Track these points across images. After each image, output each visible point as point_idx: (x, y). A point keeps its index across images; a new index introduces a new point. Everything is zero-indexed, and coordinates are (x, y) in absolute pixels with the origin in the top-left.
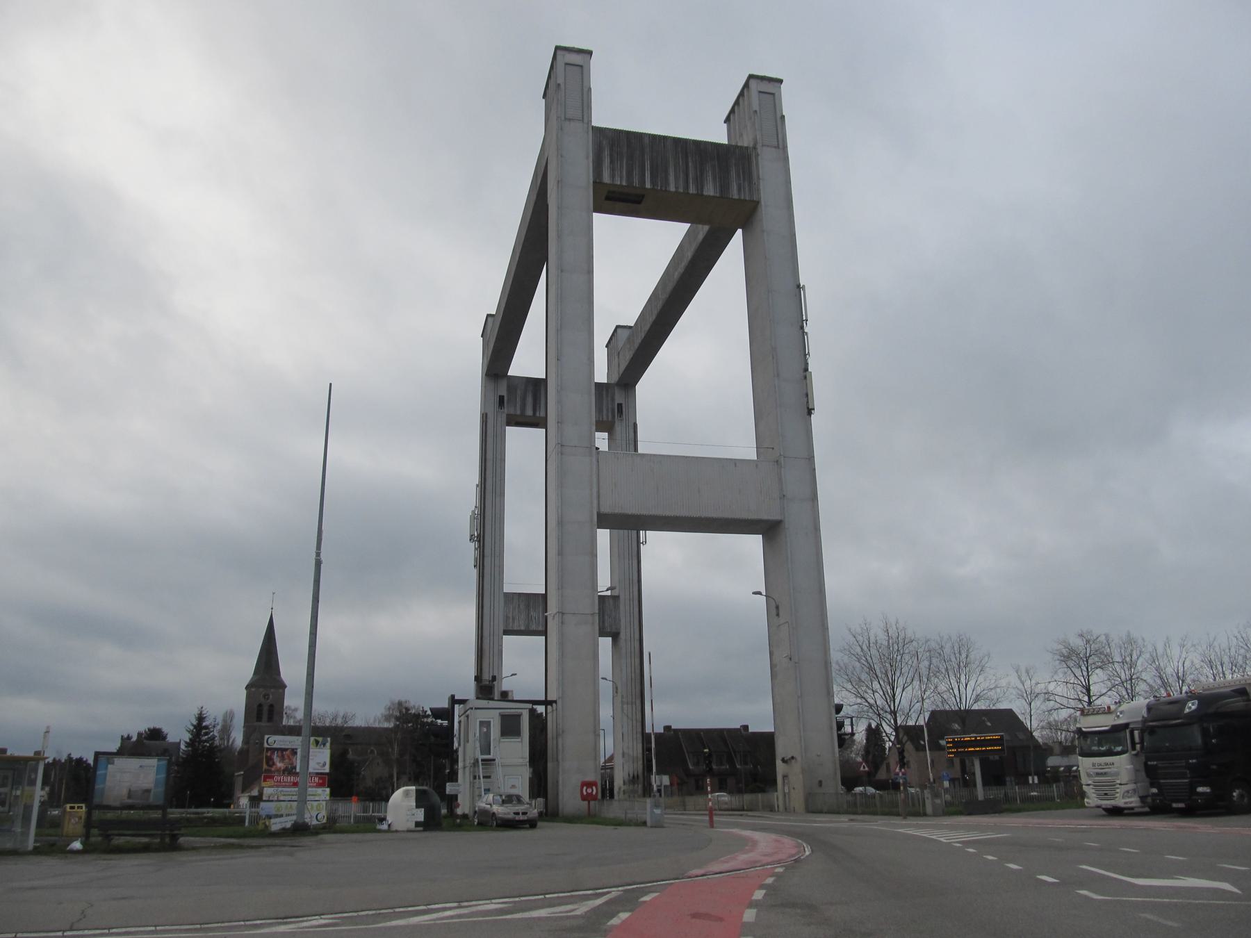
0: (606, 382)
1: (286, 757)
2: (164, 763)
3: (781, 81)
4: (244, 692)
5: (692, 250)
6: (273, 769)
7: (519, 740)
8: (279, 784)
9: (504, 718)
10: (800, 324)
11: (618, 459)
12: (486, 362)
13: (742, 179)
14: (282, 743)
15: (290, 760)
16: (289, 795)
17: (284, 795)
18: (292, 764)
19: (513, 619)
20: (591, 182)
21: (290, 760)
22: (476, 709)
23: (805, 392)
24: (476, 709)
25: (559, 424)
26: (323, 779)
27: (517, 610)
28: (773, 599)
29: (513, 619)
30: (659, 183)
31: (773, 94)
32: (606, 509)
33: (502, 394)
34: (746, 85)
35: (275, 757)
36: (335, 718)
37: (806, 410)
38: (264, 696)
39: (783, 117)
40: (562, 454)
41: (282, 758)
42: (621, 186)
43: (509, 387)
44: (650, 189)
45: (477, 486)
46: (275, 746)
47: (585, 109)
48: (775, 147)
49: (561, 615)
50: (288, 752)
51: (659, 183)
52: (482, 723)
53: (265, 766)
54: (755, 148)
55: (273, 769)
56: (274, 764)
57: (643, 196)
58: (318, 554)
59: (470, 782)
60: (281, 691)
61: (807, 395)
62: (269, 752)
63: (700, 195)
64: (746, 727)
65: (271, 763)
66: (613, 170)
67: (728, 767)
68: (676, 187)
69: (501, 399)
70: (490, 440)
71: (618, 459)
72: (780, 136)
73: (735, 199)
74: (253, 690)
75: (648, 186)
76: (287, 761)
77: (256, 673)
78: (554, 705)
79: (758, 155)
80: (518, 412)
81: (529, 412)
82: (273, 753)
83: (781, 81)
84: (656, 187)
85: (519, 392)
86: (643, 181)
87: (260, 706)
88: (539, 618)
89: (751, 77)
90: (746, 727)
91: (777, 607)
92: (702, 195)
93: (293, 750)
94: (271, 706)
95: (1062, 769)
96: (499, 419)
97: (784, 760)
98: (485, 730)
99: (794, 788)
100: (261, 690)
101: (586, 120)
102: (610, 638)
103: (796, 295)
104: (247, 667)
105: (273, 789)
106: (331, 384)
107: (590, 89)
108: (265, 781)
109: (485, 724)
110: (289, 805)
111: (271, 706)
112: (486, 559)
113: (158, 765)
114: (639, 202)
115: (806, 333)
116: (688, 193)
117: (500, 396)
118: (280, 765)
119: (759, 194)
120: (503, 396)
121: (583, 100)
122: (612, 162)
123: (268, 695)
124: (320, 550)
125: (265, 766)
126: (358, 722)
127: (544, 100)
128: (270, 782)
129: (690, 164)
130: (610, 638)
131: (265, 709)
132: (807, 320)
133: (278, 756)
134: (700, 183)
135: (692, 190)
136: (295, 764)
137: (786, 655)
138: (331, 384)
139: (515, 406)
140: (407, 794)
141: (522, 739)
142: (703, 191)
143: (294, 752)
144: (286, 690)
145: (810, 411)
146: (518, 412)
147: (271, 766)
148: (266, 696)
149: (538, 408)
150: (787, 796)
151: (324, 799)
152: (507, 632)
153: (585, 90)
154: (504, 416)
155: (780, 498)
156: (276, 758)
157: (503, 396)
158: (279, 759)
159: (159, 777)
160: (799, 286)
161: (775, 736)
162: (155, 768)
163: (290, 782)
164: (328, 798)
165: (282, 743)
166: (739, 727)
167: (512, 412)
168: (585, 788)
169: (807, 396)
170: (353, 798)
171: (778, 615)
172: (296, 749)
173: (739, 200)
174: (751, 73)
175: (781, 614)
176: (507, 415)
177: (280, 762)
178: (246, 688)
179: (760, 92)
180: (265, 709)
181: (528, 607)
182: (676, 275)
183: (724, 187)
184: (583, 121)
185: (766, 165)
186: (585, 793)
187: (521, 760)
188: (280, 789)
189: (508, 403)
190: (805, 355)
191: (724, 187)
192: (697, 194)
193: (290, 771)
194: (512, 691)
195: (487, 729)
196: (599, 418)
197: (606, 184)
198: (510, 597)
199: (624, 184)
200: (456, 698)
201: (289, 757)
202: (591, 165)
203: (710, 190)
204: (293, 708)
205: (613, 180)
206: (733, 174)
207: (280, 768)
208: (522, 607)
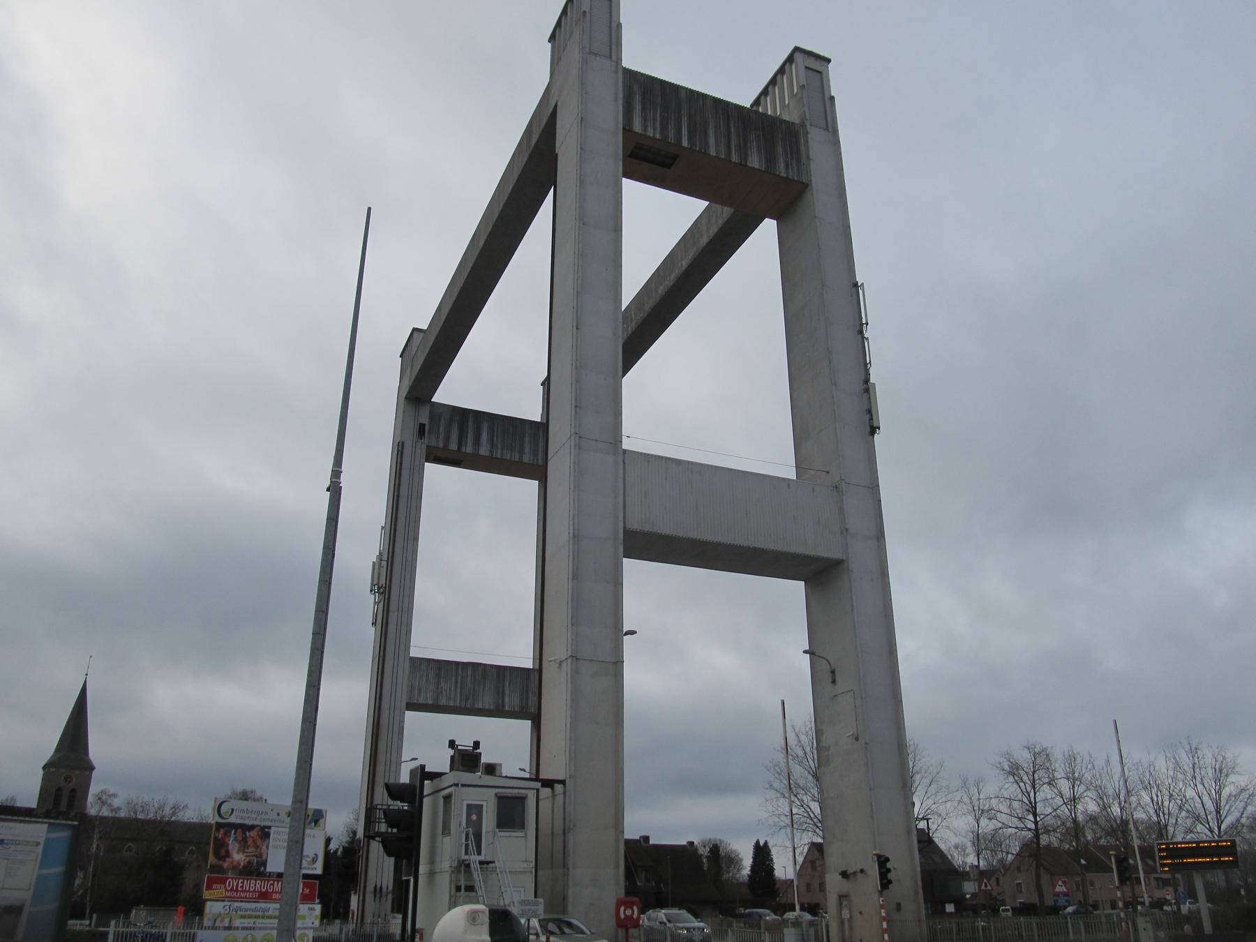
0: (539, 421)
1: (250, 841)
2: (64, 834)
3: (829, 61)
4: (41, 772)
5: (690, 257)
6: (225, 865)
7: (522, 834)
8: (235, 894)
9: (501, 799)
10: (858, 328)
11: (648, 461)
12: (407, 383)
13: (789, 156)
14: (244, 815)
15: (257, 847)
16: (250, 917)
17: (243, 917)
18: (261, 856)
19: (420, 690)
20: (621, 126)
21: (257, 847)
22: (462, 785)
23: (866, 407)
24: (462, 785)
25: (578, 409)
26: (311, 887)
27: (424, 679)
28: (827, 660)
29: (420, 690)
30: (698, 144)
31: (820, 73)
32: (634, 525)
33: (424, 422)
34: (790, 60)
35: (231, 841)
36: (161, 807)
37: (868, 429)
38: (66, 778)
39: (832, 98)
40: (579, 448)
41: (244, 845)
42: (654, 139)
43: (431, 413)
44: (687, 148)
45: (382, 528)
46: (233, 819)
47: (614, 47)
48: (824, 129)
49: (575, 659)
50: (254, 833)
51: (698, 144)
52: (470, 807)
53: (212, 859)
54: (803, 125)
55: (225, 865)
56: (228, 855)
57: (675, 157)
58: (336, 473)
59: (451, 896)
60: (87, 773)
61: (869, 412)
62: (222, 831)
63: (743, 165)
64: (646, 839)
65: (223, 853)
66: (645, 119)
67: (654, 884)
68: (717, 153)
69: (422, 427)
70: (405, 473)
71: (648, 461)
72: (829, 118)
73: (783, 177)
74: (52, 770)
75: (685, 143)
76: (251, 850)
77: (58, 749)
78: (558, 787)
79: (807, 133)
80: (441, 445)
81: (453, 446)
82: (227, 834)
83: (829, 61)
84: (694, 148)
85: (443, 422)
86: (679, 139)
87: (59, 789)
88: (450, 690)
89: (797, 49)
90: (646, 839)
91: (833, 672)
92: (746, 166)
93: (263, 828)
94: (73, 791)
95: (968, 896)
96: (418, 451)
97: (844, 875)
98: (474, 817)
99: (861, 913)
100: (63, 770)
101: (614, 58)
102: (529, 722)
103: (851, 295)
104: (49, 739)
105: (222, 904)
106: (369, 209)
107: (619, 25)
108: (209, 888)
109: (475, 810)
110: (249, 938)
111: (73, 791)
112: (390, 614)
113: (47, 841)
114: (669, 166)
115: (867, 339)
116: (730, 161)
117: (420, 424)
118: (238, 857)
119: (808, 173)
120: (424, 425)
121: (611, 35)
122: (643, 109)
123: (70, 777)
124: (340, 466)
125: (212, 859)
126: (190, 815)
127: (550, 44)
128: (219, 891)
129: (732, 130)
130: (529, 722)
131: (65, 794)
132: (867, 324)
133: (236, 839)
134: (743, 150)
135: (735, 158)
136: (264, 857)
137: (851, 733)
138: (369, 209)
139: (438, 438)
140: (473, 917)
141: (526, 834)
142: (746, 162)
143: (265, 833)
144: (94, 773)
145: (873, 430)
146: (441, 445)
147: (223, 858)
148: (68, 779)
149: (464, 443)
150: (846, 923)
151: (310, 925)
152: (412, 706)
153: (614, 26)
154: (424, 447)
155: (842, 533)
156: (233, 846)
157: (424, 425)
158: (237, 846)
159: (45, 872)
160: (856, 285)
161: (824, 847)
162: (40, 849)
163: (254, 891)
164: (317, 923)
165: (244, 815)
166: (638, 838)
167: (433, 443)
168: (622, 909)
169: (870, 412)
170: (180, 908)
171: (834, 682)
172: (269, 827)
173: (787, 178)
174: (798, 45)
175: (838, 679)
176: (428, 447)
177: (239, 851)
178: (43, 768)
179: (806, 67)
180: (65, 794)
181: (438, 676)
182: (661, 290)
183: (770, 160)
184: (610, 57)
185: (815, 140)
186: (622, 916)
187: (525, 865)
188: (236, 904)
189: (429, 433)
190: (865, 367)
191: (770, 160)
192: (740, 164)
193: (255, 870)
194: (501, 765)
195: (478, 817)
196: (533, 460)
197: (637, 133)
198: (417, 663)
199: (658, 136)
200: (426, 770)
201: (254, 842)
202: (621, 108)
203: (755, 162)
204: (111, 793)
205: (645, 131)
206: (780, 149)
207: (239, 863)
208: (431, 675)
